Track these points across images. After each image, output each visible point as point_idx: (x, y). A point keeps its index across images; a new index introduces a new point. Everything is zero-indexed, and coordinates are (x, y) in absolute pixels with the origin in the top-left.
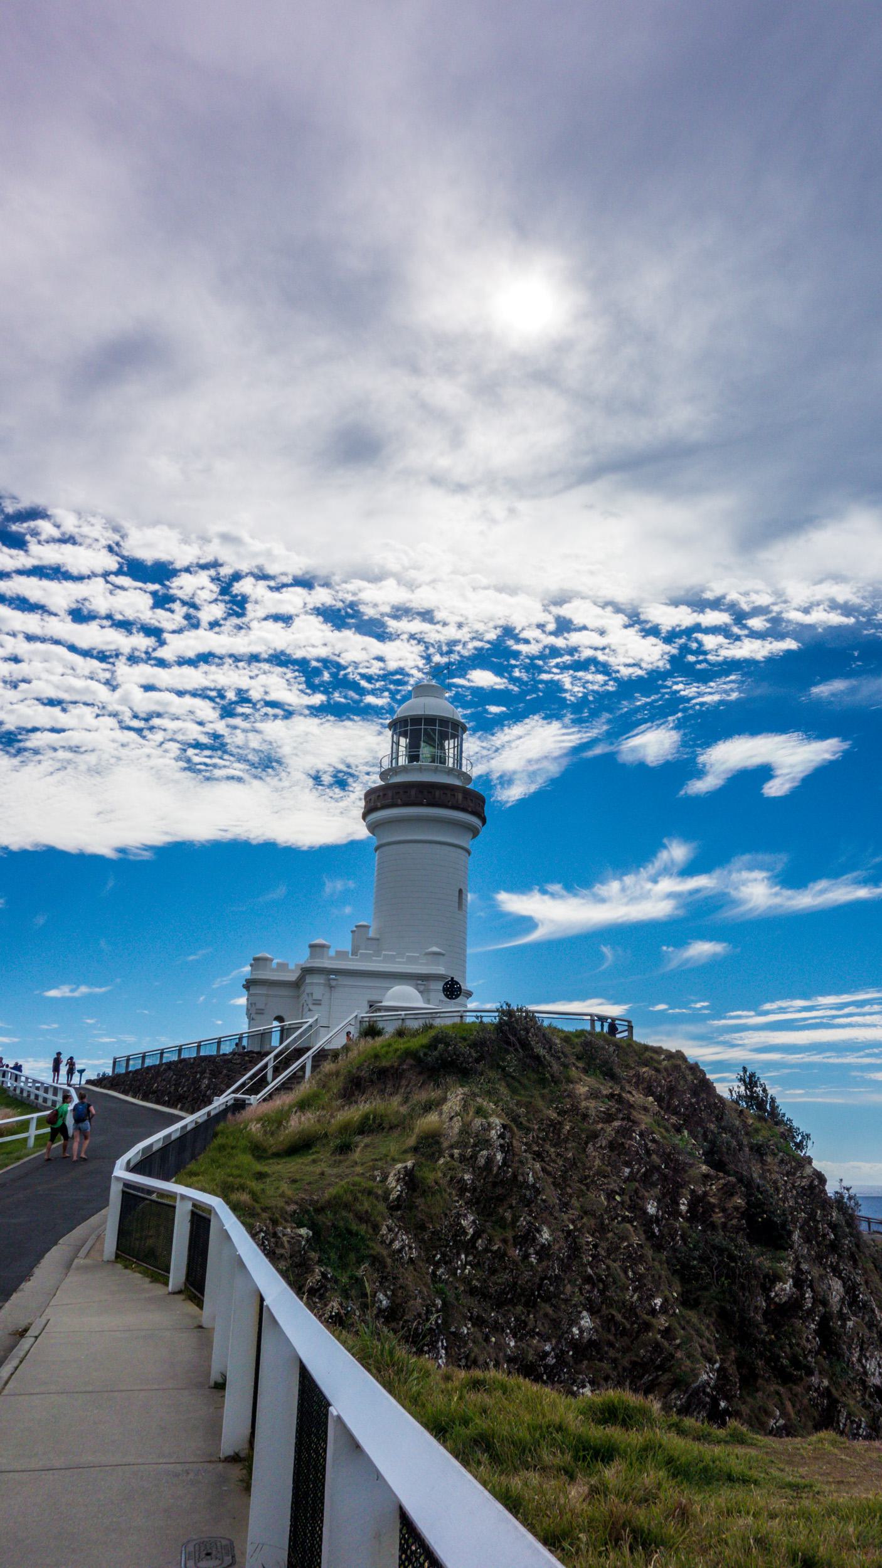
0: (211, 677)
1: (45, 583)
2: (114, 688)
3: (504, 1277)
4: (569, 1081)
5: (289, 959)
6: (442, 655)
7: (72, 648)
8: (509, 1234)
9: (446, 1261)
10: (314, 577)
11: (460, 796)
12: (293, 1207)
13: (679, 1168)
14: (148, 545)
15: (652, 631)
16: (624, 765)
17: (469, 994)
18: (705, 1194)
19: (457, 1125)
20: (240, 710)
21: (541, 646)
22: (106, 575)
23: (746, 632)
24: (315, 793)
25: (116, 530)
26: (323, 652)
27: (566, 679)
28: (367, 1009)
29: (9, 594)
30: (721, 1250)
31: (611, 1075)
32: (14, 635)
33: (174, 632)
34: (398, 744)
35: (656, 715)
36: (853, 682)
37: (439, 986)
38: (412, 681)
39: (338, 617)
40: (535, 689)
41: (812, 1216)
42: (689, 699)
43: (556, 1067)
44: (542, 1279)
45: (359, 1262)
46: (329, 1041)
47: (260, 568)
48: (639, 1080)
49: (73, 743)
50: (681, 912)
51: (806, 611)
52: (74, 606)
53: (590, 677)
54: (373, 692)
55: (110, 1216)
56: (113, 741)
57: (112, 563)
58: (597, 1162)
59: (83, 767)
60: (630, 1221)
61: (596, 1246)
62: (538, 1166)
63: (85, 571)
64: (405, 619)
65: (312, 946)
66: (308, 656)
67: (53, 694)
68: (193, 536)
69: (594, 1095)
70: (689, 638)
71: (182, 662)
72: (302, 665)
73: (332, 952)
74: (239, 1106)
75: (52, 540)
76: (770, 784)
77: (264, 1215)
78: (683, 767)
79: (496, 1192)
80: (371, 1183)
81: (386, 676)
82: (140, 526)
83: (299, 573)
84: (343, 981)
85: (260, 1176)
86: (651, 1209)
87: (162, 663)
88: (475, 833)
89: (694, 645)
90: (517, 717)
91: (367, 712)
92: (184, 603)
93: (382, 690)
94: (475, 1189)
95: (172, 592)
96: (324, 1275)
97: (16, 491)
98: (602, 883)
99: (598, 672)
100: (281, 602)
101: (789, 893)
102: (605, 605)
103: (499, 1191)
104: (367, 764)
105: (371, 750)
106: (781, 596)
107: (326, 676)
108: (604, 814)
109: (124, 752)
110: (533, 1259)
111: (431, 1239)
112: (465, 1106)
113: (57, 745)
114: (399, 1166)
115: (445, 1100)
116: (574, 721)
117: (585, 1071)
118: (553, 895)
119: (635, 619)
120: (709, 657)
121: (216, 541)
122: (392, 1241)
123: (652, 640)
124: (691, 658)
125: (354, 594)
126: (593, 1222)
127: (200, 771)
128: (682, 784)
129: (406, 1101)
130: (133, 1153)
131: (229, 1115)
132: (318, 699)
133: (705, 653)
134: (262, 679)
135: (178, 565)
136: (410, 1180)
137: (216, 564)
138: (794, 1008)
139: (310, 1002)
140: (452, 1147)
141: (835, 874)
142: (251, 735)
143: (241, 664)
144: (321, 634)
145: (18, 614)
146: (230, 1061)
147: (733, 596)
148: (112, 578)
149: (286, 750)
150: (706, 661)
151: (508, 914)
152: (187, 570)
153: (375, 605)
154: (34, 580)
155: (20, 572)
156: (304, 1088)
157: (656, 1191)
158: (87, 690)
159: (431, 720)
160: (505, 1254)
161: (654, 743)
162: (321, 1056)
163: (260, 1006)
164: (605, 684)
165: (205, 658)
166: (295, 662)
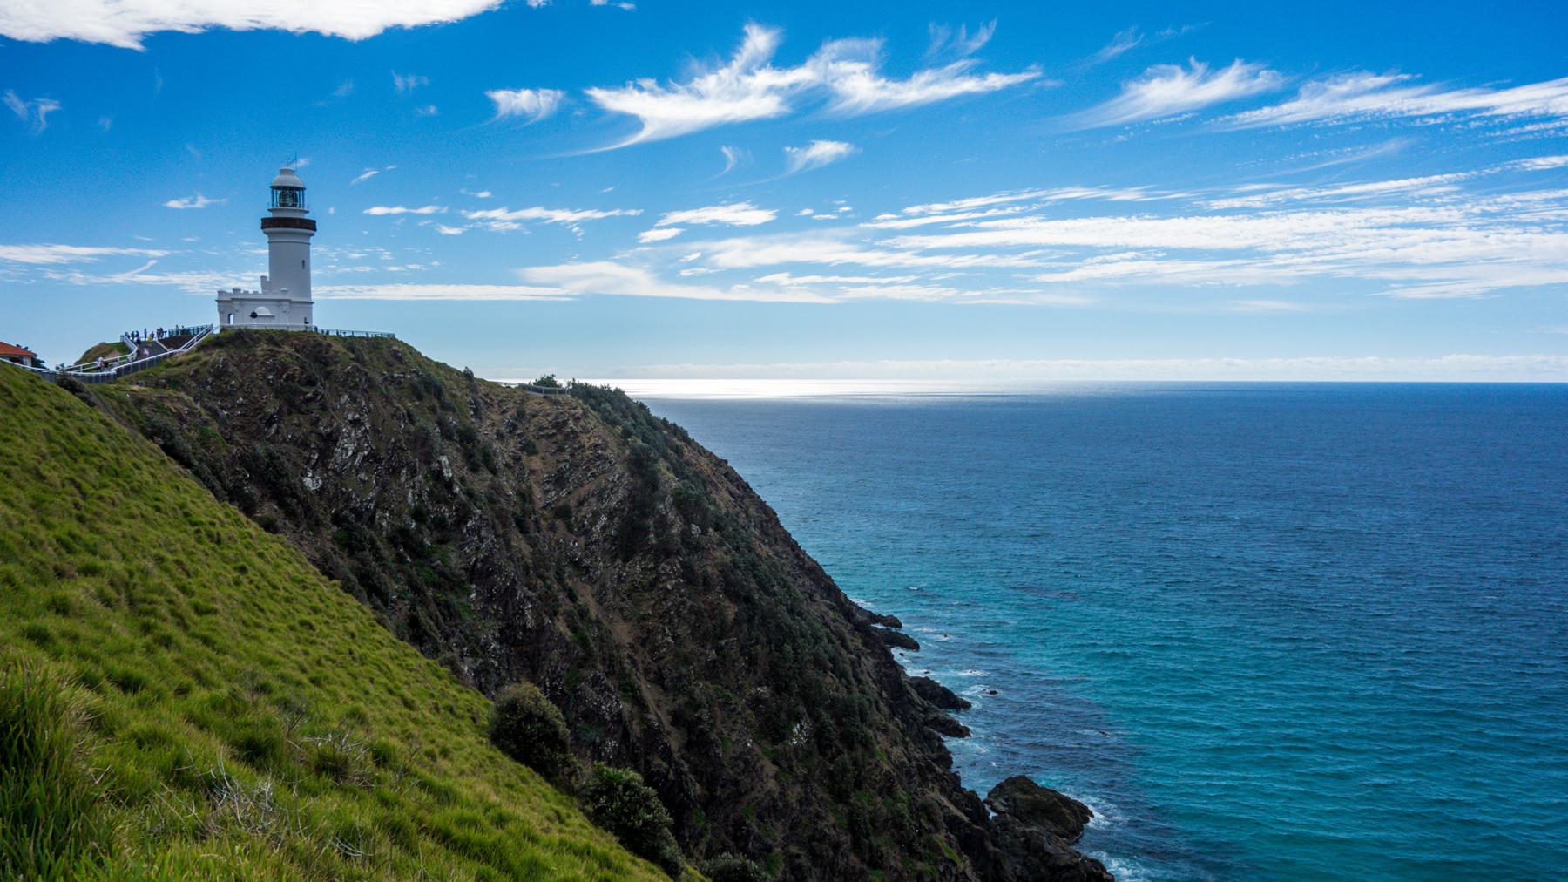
50: (786, 109)
101: (892, 86)
108: (477, 649)
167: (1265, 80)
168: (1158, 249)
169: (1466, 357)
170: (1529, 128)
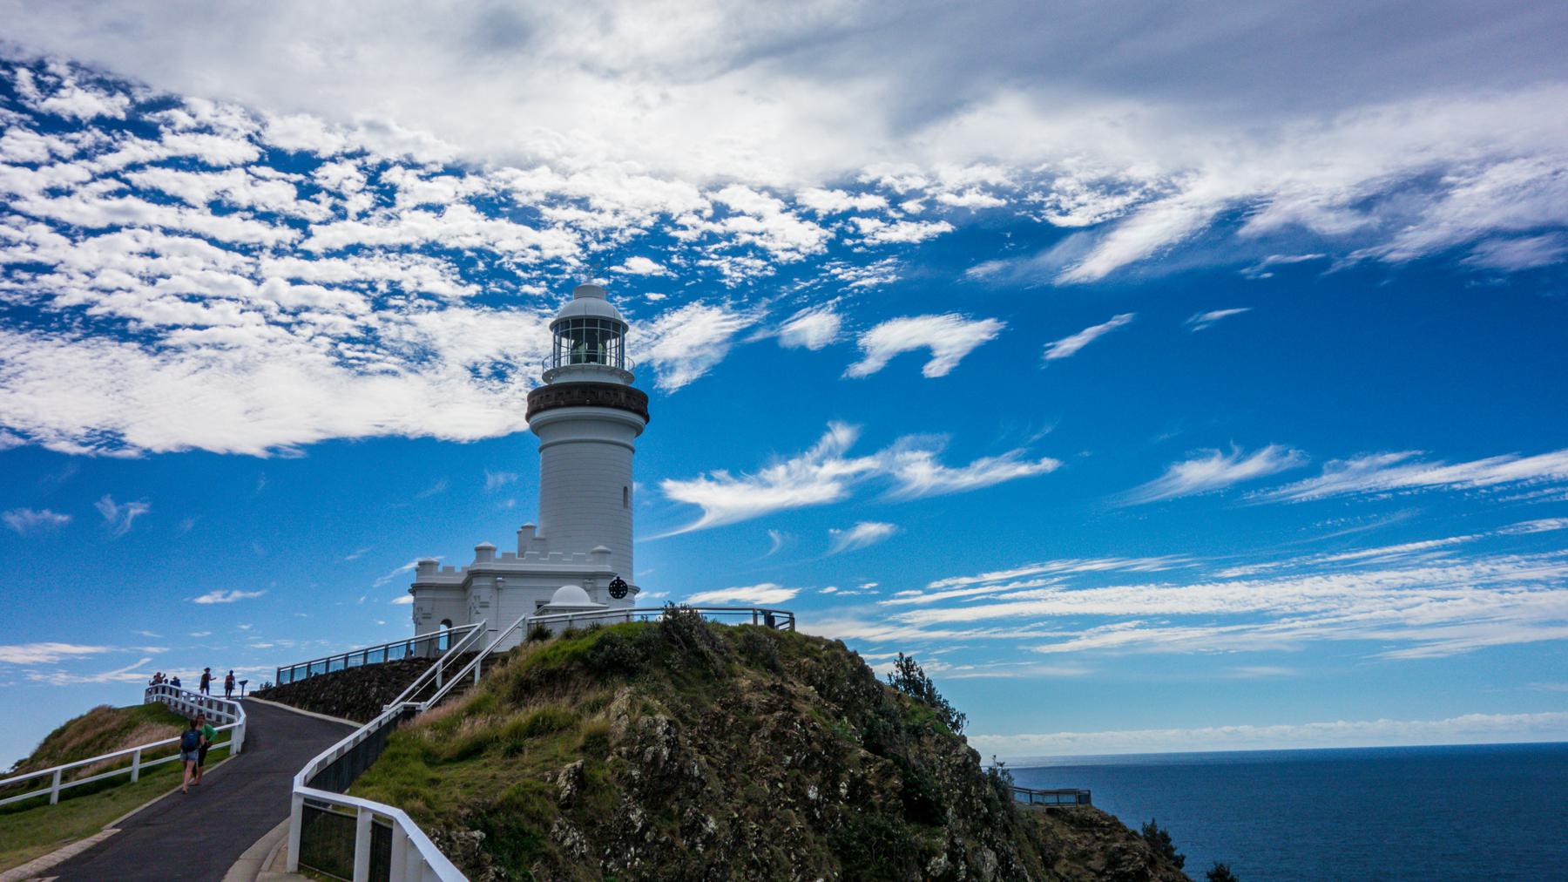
0: (361, 269)
1: (182, 175)
2: (259, 282)
3: (673, 867)
4: (733, 675)
5: (456, 561)
6: (599, 242)
7: (213, 242)
8: (677, 826)
9: (616, 854)
10: (466, 165)
11: (623, 396)
12: (466, 811)
13: (839, 754)
14: (291, 134)
15: (810, 216)
16: (785, 350)
17: (636, 590)
18: (864, 776)
19: (624, 723)
20: (392, 302)
21: (698, 232)
22: (246, 165)
23: (901, 215)
24: (474, 386)
25: (255, 118)
26: (477, 242)
27: (725, 265)
28: (534, 609)
29: (143, 186)
30: (879, 830)
31: (773, 668)
32: (150, 229)
33: (320, 223)
34: (560, 345)
35: (816, 299)
36: (1007, 263)
37: (607, 584)
38: (569, 270)
39: (489, 206)
40: (694, 276)
41: (967, 792)
42: (847, 283)
43: (719, 662)
44: (709, 867)
45: (533, 859)
46: (497, 645)
47: (409, 157)
48: (799, 671)
49: (217, 340)
50: (847, 495)
51: (959, 193)
52: (213, 198)
53: (748, 262)
54: (529, 282)
55: (292, 826)
56: (260, 337)
57: (252, 153)
58: (760, 752)
59: (229, 365)
60: (792, 806)
61: (759, 832)
62: (703, 758)
63: (226, 163)
64: (560, 207)
65: (477, 549)
66: (462, 246)
67: (193, 289)
68: (338, 125)
69: (757, 687)
70: (846, 222)
71: (330, 254)
72: (455, 255)
73: (498, 555)
74: (409, 713)
75: (187, 130)
76: (930, 365)
77: (439, 820)
78: (843, 351)
79: (663, 786)
80: (542, 784)
81: (543, 265)
82: (281, 115)
83: (449, 161)
84: (510, 582)
85: (434, 782)
86: (812, 794)
87: (309, 256)
88: (638, 430)
89: (851, 229)
90: (677, 304)
91: (525, 302)
92: (330, 193)
93: (539, 279)
94: (642, 784)
95: (317, 182)
96: (498, 874)
97: (148, 80)
98: (768, 467)
99: (756, 257)
100: (431, 191)
101: (952, 472)
102: (761, 190)
103: (667, 784)
104: (525, 354)
105: (529, 341)
106: (933, 178)
107: (481, 266)
108: (765, 399)
109: (271, 348)
110: (700, 848)
111: (601, 834)
112: (632, 705)
113: (199, 342)
114: (569, 766)
115: (611, 699)
116: (734, 307)
117: (748, 664)
118: (719, 482)
119: (791, 204)
120: (866, 241)
121: (362, 129)
122: (563, 839)
123: (809, 224)
124: (848, 242)
125: (507, 182)
126: (757, 809)
127: (352, 366)
128: (843, 368)
129: (574, 702)
130: (310, 768)
131: (399, 724)
132: (473, 289)
133: (862, 237)
134: (415, 270)
135: (323, 154)
136: (579, 778)
137: (362, 153)
138: (960, 585)
139: (477, 604)
140: (619, 745)
141: (995, 452)
142: (404, 327)
143: (392, 255)
144: (473, 224)
145: (153, 207)
146: (398, 668)
147: (887, 180)
148: (253, 169)
149: (442, 342)
150: (862, 244)
151: (673, 502)
152: (333, 159)
153: (529, 193)
154: (169, 172)
155: (154, 164)
156: (474, 694)
157: (817, 777)
158: (230, 285)
159: (592, 321)
160: (672, 845)
161: (814, 327)
162: (490, 659)
163: (427, 610)
164: (764, 269)
165: (354, 250)
166: (448, 252)
167: (1293, 458)
168: (1163, 616)
169: (1286, 728)
170: (1547, 491)
